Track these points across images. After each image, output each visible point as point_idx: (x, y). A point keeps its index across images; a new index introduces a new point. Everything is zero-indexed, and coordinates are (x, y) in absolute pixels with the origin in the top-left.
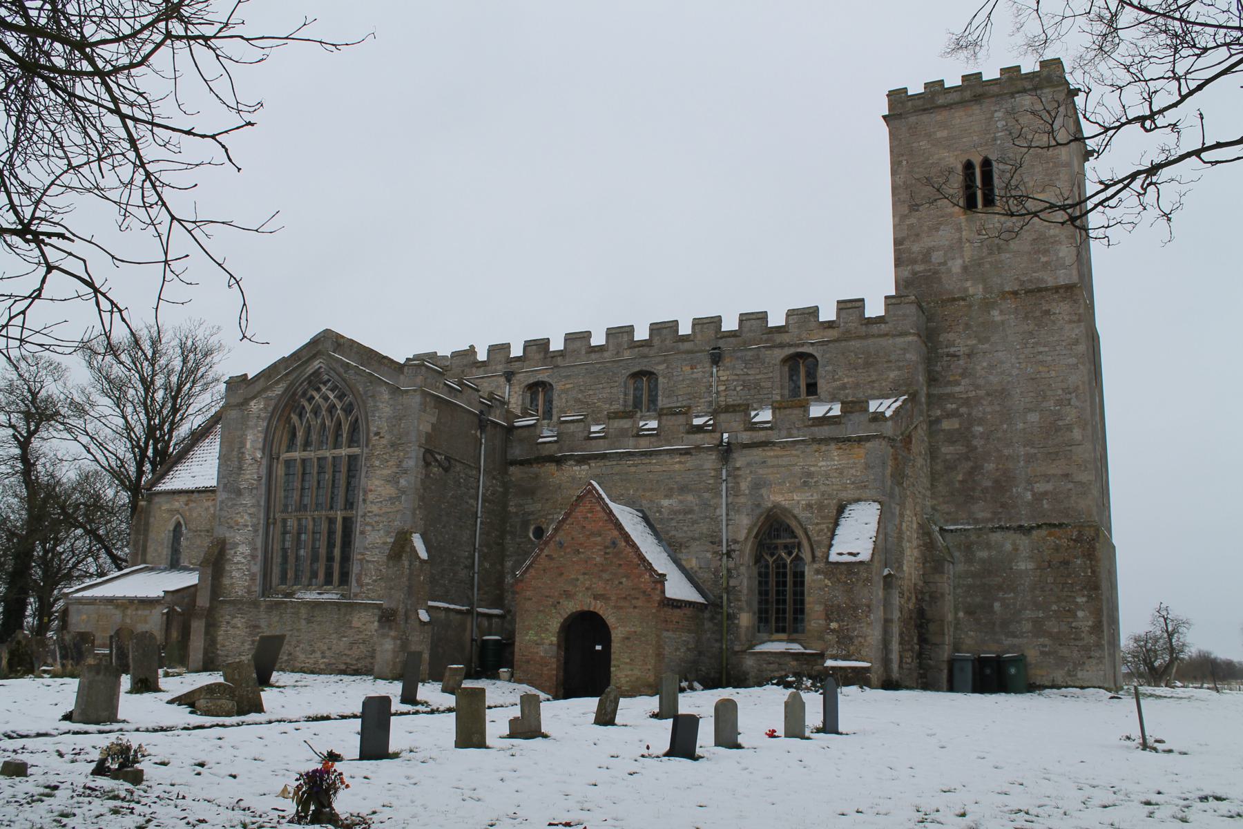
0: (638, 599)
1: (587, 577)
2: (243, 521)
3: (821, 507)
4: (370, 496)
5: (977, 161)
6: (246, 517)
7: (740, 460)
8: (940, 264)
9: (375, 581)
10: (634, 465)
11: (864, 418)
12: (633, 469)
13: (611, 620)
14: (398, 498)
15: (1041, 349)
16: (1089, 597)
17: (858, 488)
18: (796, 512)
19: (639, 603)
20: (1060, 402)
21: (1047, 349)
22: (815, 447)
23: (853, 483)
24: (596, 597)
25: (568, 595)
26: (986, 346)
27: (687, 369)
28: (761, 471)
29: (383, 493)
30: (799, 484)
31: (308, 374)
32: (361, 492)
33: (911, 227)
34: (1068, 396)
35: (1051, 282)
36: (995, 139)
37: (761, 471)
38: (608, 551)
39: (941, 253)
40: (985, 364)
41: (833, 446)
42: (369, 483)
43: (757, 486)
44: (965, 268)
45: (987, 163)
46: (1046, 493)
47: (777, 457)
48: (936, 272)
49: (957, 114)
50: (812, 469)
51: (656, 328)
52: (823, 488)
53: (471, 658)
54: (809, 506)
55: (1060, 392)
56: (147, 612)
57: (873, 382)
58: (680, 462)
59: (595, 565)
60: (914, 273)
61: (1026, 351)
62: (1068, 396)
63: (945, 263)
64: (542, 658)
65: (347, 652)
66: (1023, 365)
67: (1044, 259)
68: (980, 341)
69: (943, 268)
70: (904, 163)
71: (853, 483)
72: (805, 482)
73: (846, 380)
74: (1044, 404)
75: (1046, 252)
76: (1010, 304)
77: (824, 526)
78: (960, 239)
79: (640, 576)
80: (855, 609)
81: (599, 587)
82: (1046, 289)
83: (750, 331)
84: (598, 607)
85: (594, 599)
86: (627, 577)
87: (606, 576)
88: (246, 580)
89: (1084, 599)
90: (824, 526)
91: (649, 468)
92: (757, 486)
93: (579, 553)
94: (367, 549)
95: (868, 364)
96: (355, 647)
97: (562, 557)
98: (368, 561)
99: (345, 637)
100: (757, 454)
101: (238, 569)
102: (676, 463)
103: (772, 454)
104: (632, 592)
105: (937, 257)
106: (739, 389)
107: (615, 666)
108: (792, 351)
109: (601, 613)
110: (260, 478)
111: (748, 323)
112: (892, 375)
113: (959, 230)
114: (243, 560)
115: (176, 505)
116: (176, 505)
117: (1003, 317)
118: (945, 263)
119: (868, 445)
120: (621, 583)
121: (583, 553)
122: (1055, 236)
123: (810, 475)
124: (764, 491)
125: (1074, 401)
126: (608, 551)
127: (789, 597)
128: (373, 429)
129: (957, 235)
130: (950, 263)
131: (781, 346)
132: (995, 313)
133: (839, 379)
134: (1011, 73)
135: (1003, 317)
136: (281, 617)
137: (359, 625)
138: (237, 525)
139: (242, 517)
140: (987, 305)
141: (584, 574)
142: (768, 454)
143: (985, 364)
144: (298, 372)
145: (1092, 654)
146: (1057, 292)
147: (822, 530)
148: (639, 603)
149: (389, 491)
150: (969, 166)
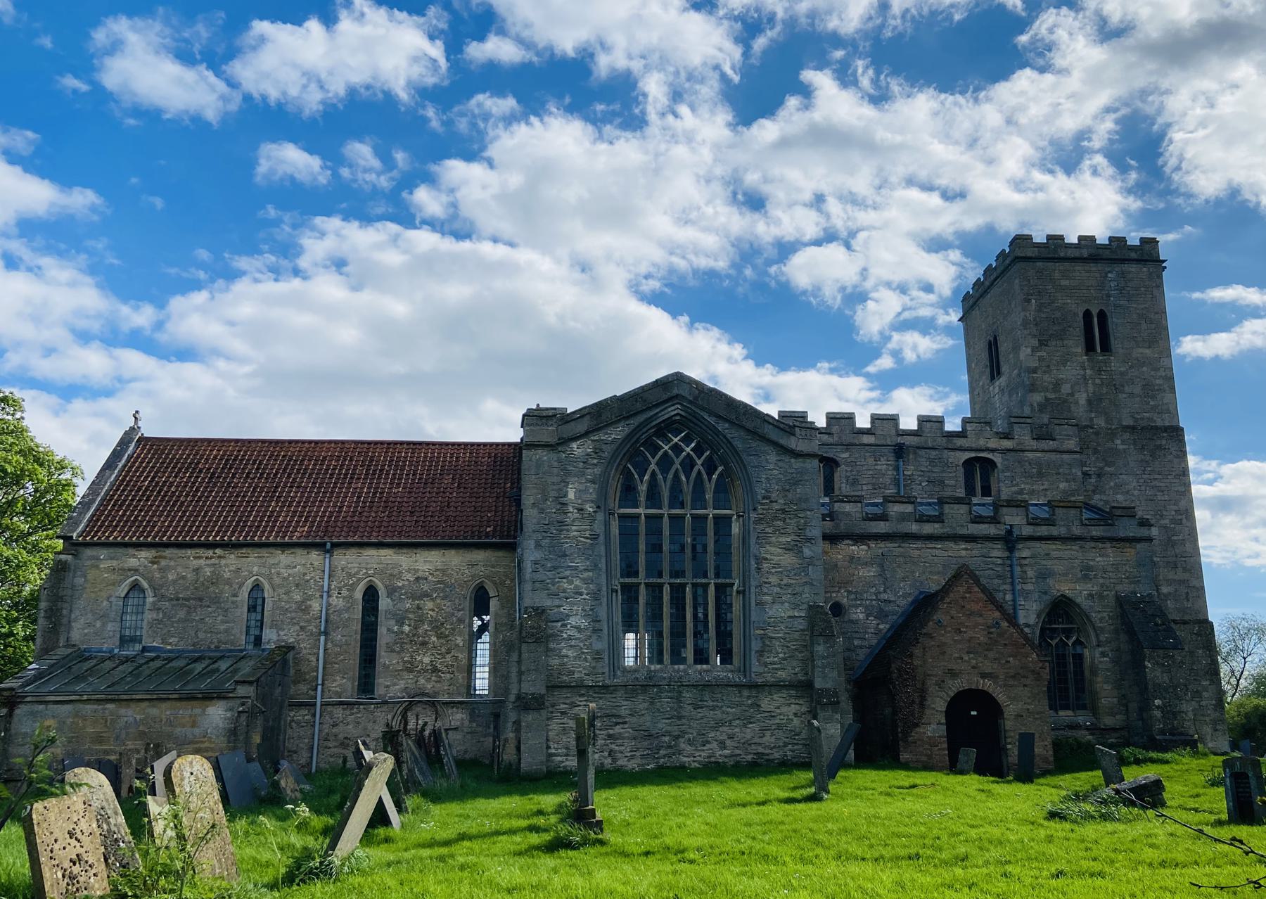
1: (972, 656)
2: (572, 587)
4: (765, 565)
5: (1095, 312)
6: (577, 582)
7: (1024, 552)
9: (784, 659)
10: (917, 549)
11: (1134, 522)
13: (1001, 697)
14: (805, 569)
15: (1157, 476)
16: (1211, 680)
17: (1131, 583)
18: (1078, 600)
19: (1028, 682)
20: (1173, 521)
21: (1160, 477)
23: (1127, 578)
24: (984, 676)
25: (954, 674)
26: (1112, 469)
27: (871, 461)
28: (1044, 562)
30: (1080, 576)
33: (1041, 359)
34: (1180, 517)
35: (1159, 423)
37: (1044, 562)
38: (992, 630)
39: (1069, 385)
40: (1112, 484)
41: (1108, 545)
42: (762, 550)
43: (1043, 576)
48: (1065, 401)
49: (1077, 268)
50: (1091, 563)
51: (832, 418)
54: (1091, 596)
55: (1173, 513)
56: (198, 711)
57: (1046, 490)
58: (966, 549)
59: (979, 644)
60: (1047, 399)
61: (1145, 476)
62: (1180, 517)
63: (1072, 394)
66: (1143, 488)
67: (1152, 403)
68: (1108, 464)
69: (1071, 399)
70: (1033, 301)
71: (1127, 578)
72: (1085, 575)
73: (1023, 486)
74: (1162, 522)
75: (1153, 397)
76: (1127, 436)
77: (1105, 614)
80: (1175, 688)
81: (988, 667)
82: (1157, 428)
84: (987, 685)
85: (982, 677)
86: (1015, 656)
87: (991, 655)
88: (586, 660)
89: (1208, 683)
90: (1105, 614)
92: (1043, 576)
93: (961, 632)
94: (769, 624)
95: (1040, 475)
96: (768, 734)
97: (943, 635)
99: (751, 723)
100: (1041, 547)
101: (571, 646)
102: (963, 549)
103: (1054, 547)
104: (1021, 671)
105: (1066, 389)
106: (924, 484)
107: (943, 749)
108: (973, 455)
109: (990, 691)
110: (594, 537)
111: (928, 425)
112: (1063, 485)
114: (578, 635)
117: (1124, 447)
118: (1072, 394)
119: (1139, 546)
121: (965, 632)
122: (1160, 385)
123: (1089, 568)
124: (1051, 582)
126: (992, 630)
127: (1071, 676)
128: (760, 492)
129: (1082, 372)
131: (961, 449)
133: (1017, 485)
134: (1087, 241)
135: (1124, 447)
136: (652, 703)
137: (772, 708)
140: (1112, 434)
142: (1051, 547)
143: (1112, 484)
144: (658, 410)
145: (1218, 727)
146: (1166, 431)
148: (1028, 682)
149: (788, 560)
150: (1087, 314)
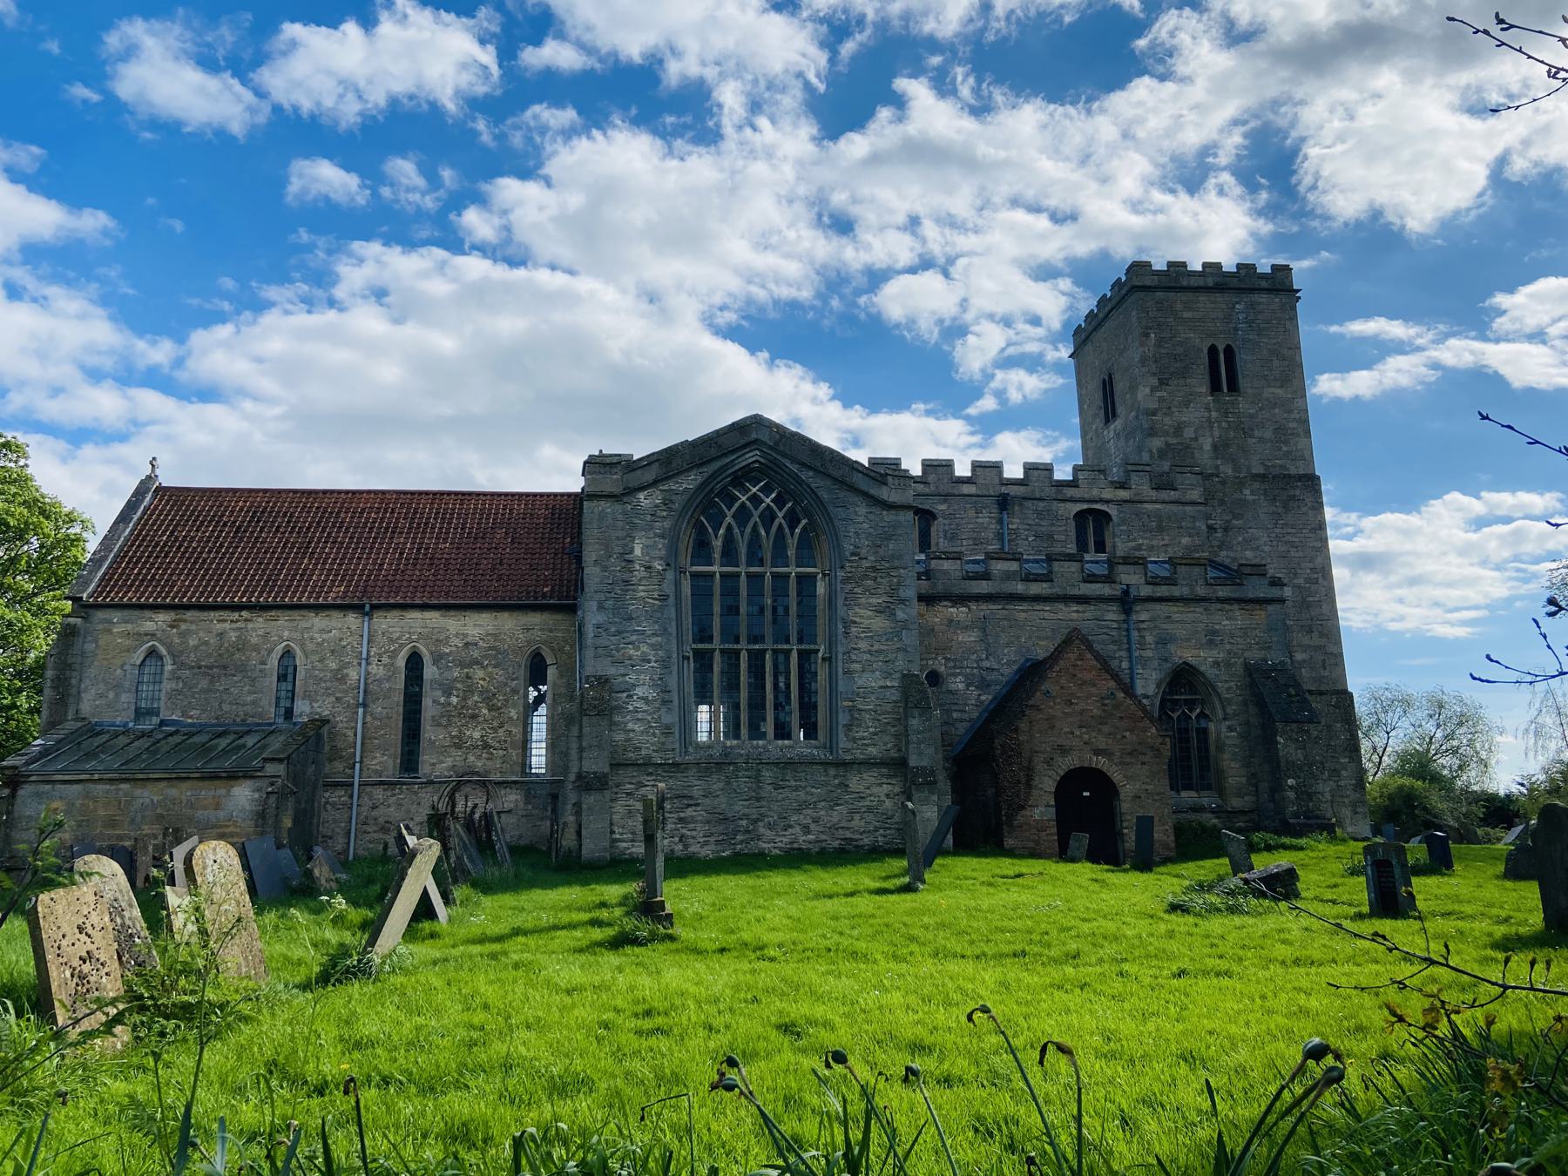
0: (1145, 754)
3: (1229, 665)
6: (645, 648)
8: (1191, 439)
9: (875, 734)
10: (1023, 611)
12: (1024, 615)
13: (1116, 776)
16: (1350, 757)
17: (1262, 649)
18: (1202, 668)
22: (1219, 606)
24: (1097, 752)
25: (1063, 750)
27: (972, 513)
28: (1164, 626)
29: (874, 627)
30: (1204, 641)
31: (737, 467)
32: (840, 626)
33: (1161, 400)
35: (1293, 471)
36: (1236, 329)
37: (1164, 626)
41: (1236, 607)
43: (1163, 641)
44: (1215, 447)
45: (1229, 351)
46: (1304, 661)
47: (1181, 612)
52: (1228, 647)
53: (464, 843)
54: (1216, 664)
58: (1078, 612)
61: (1277, 531)
63: (1196, 439)
64: (1037, 822)
65: (844, 824)
67: (1285, 449)
68: (1236, 517)
75: (1286, 442)
78: (1209, 418)
79: (1145, 730)
81: (1101, 742)
82: (1290, 476)
83: (1037, 481)
84: (1101, 762)
86: (1132, 731)
87: (1106, 729)
88: (654, 735)
89: (1347, 760)
91: (1041, 614)
95: (1160, 529)
98: (860, 710)
100: (1161, 609)
105: (1189, 433)
108: (1085, 506)
110: (664, 598)
112: (1185, 541)
113: (1208, 409)
115: (149, 626)
116: (149, 626)
118: (1196, 439)
119: (1270, 608)
120: (1124, 737)
123: (1214, 633)
124: (1172, 648)
125: (1320, 580)
129: (1206, 414)
130: (1201, 440)
132: (1247, 492)
133: (1134, 540)
136: (728, 783)
138: (630, 659)
139: (638, 649)
140: (1241, 484)
141: (1080, 727)
145: (1358, 810)
147: (1230, 688)
149: (879, 623)
150: (1213, 351)
